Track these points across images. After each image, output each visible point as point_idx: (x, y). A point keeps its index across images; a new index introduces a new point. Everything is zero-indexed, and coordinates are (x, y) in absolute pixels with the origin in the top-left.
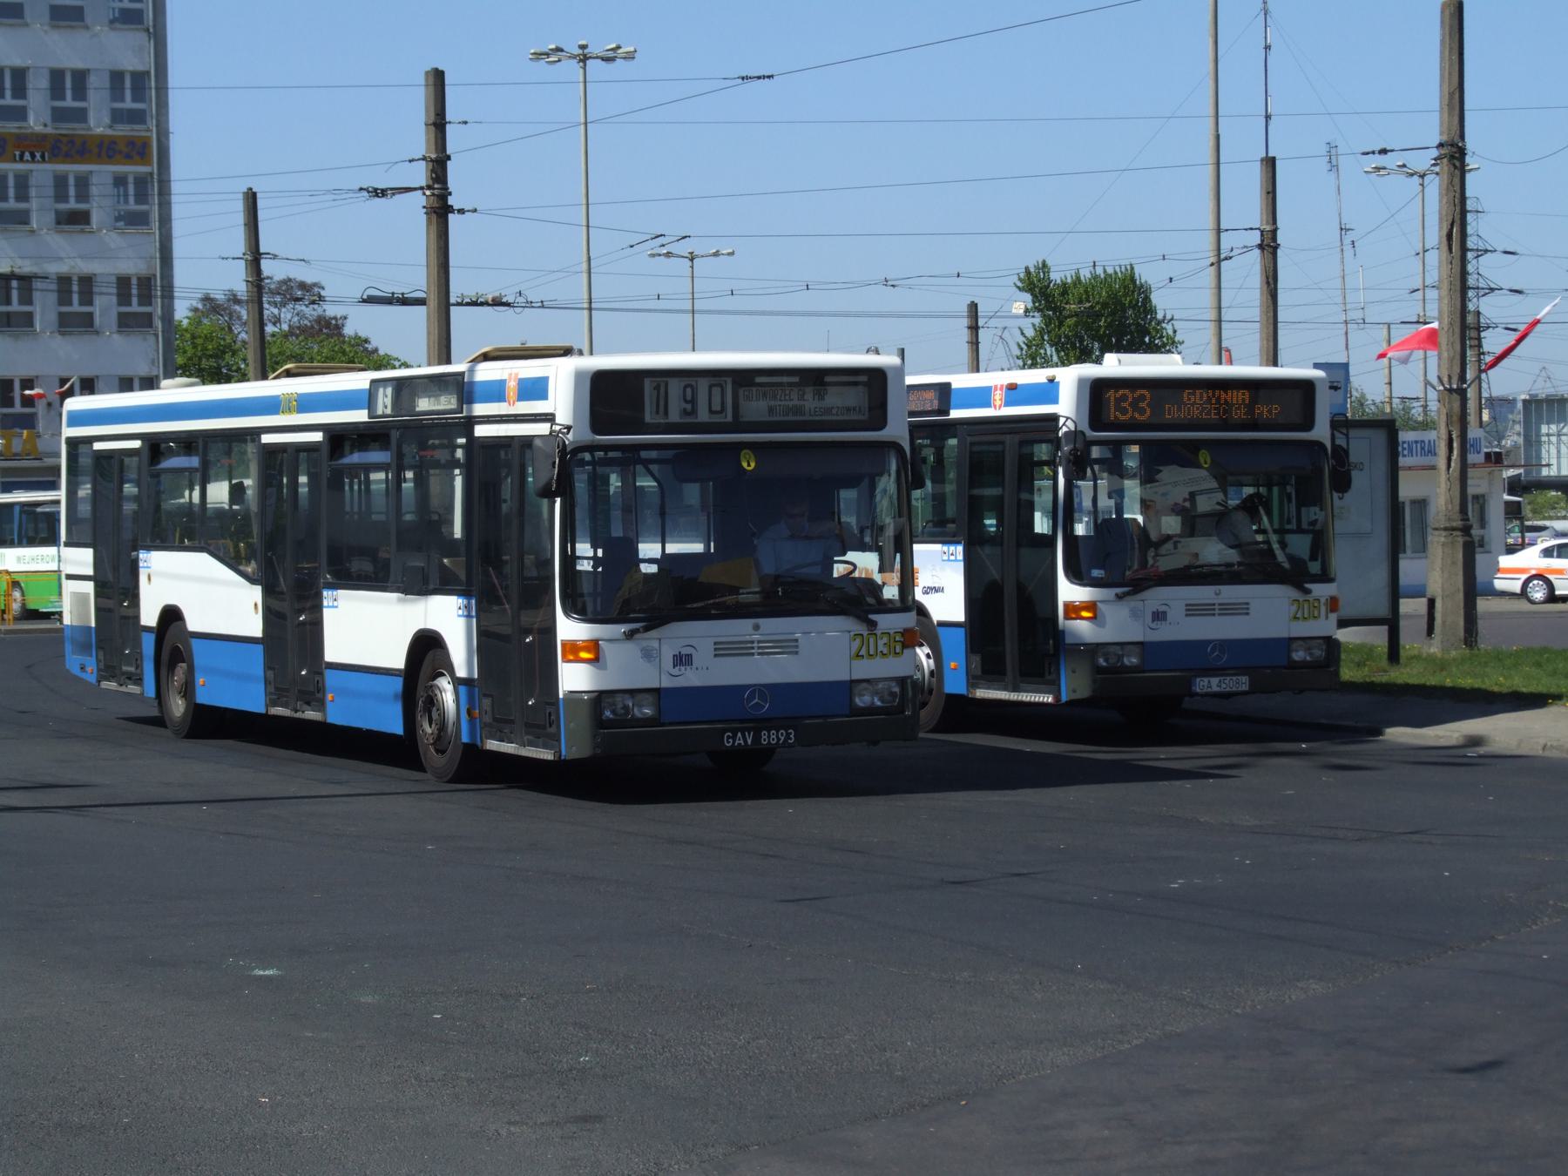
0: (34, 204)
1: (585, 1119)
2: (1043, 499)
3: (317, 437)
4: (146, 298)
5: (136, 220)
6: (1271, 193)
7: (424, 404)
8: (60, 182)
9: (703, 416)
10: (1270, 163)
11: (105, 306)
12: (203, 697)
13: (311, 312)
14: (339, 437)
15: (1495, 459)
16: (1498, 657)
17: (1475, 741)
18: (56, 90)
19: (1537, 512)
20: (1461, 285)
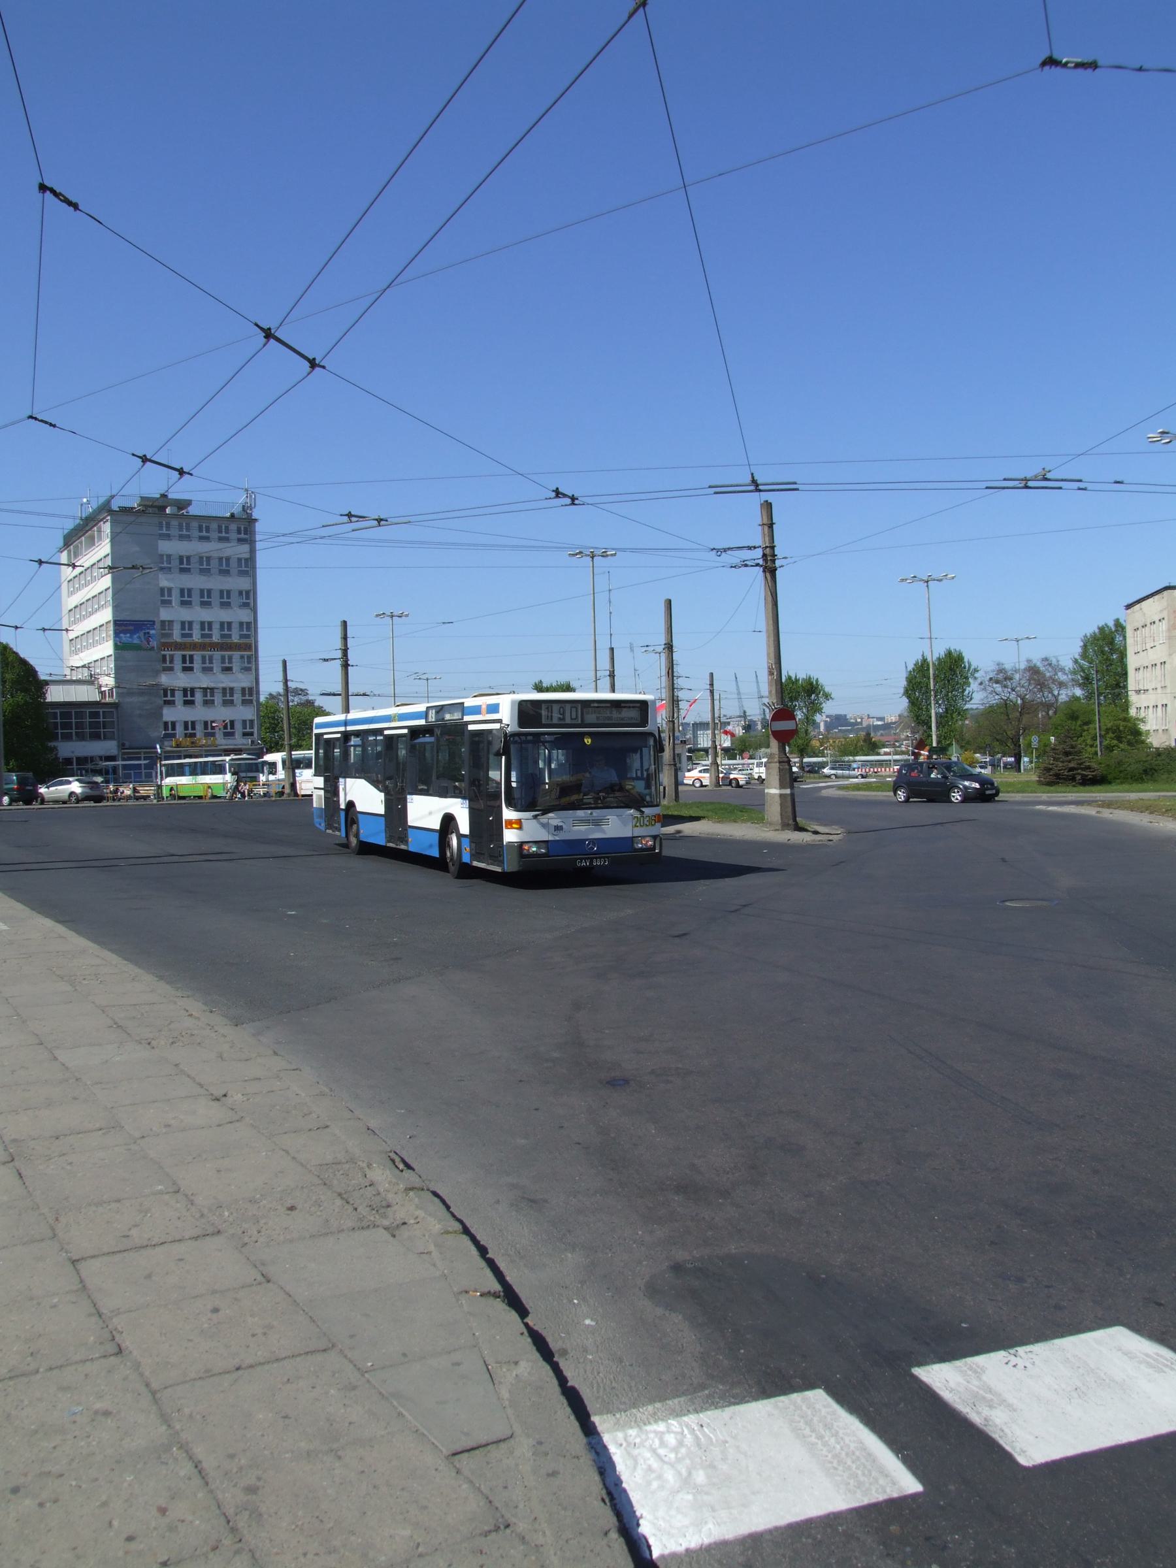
0: (214, 665)
1: (397, 959)
2: (542, 757)
3: (405, 731)
4: (251, 694)
5: (248, 669)
6: (612, 659)
7: (448, 717)
8: (223, 658)
9: (568, 721)
10: (612, 649)
11: (237, 697)
12: (363, 838)
13: (304, 698)
14: (415, 732)
15: (684, 742)
16: (686, 805)
17: (679, 832)
18: (222, 628)
19: (697, 759)
20: (672, 688)
